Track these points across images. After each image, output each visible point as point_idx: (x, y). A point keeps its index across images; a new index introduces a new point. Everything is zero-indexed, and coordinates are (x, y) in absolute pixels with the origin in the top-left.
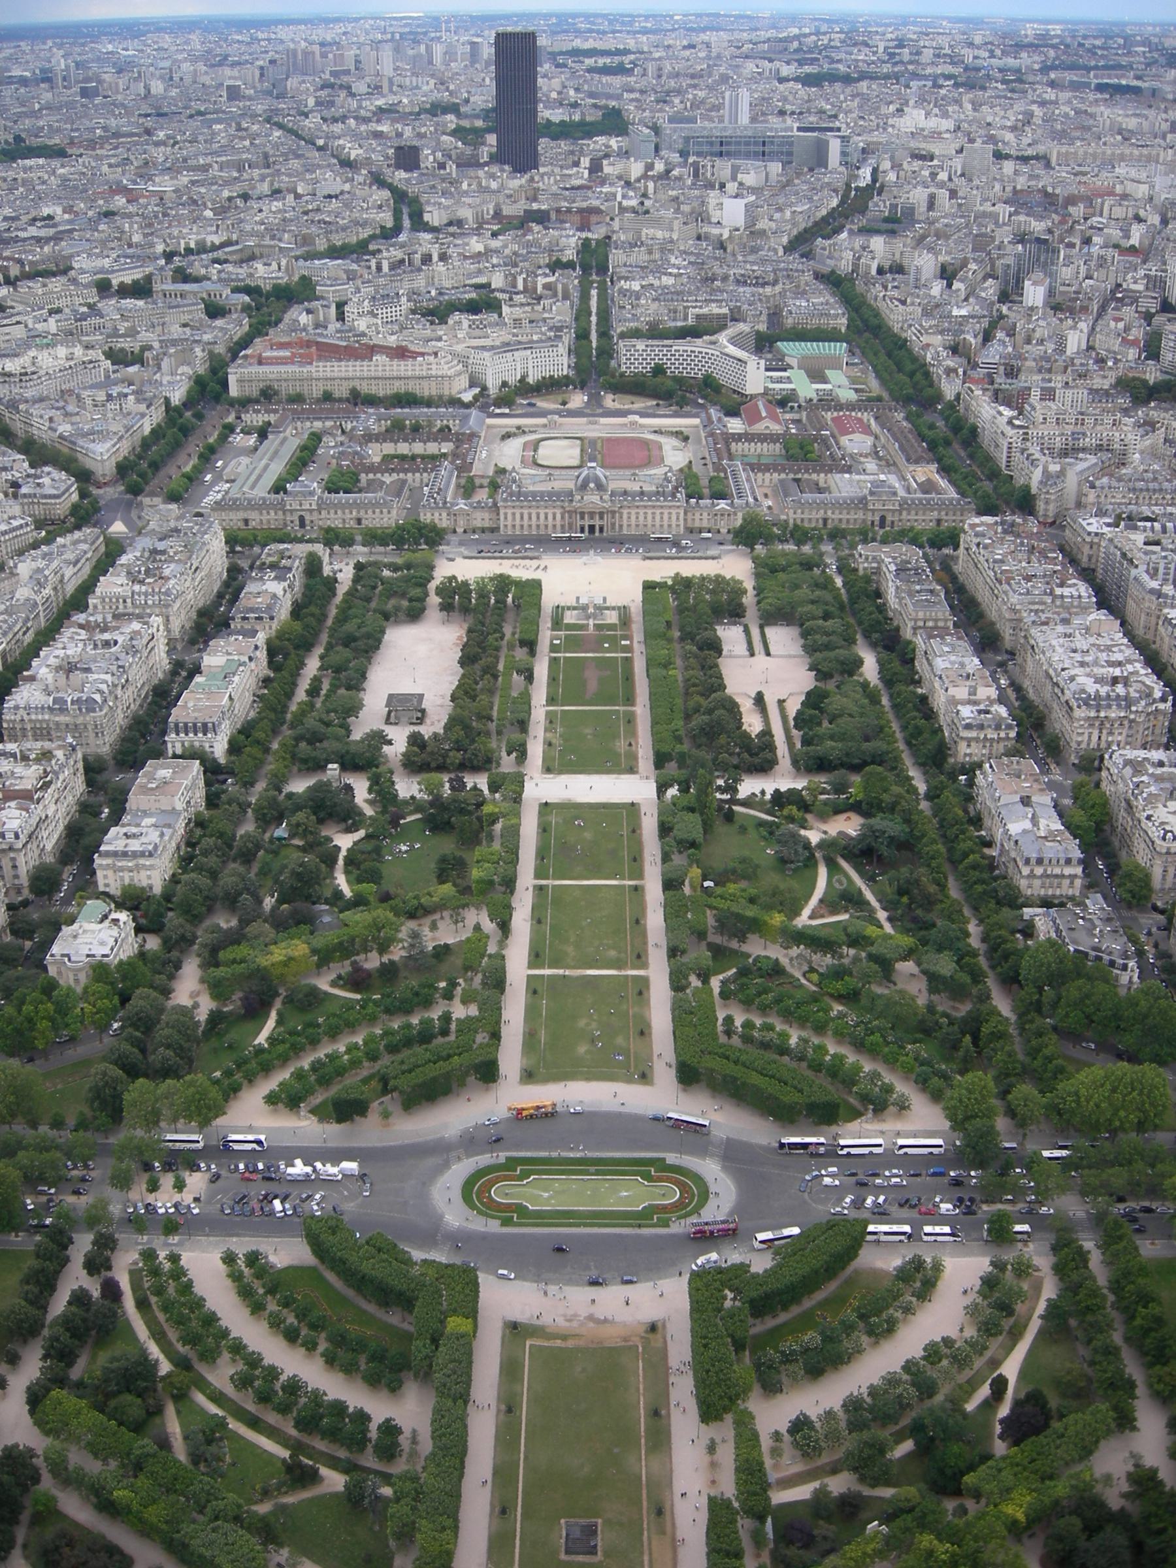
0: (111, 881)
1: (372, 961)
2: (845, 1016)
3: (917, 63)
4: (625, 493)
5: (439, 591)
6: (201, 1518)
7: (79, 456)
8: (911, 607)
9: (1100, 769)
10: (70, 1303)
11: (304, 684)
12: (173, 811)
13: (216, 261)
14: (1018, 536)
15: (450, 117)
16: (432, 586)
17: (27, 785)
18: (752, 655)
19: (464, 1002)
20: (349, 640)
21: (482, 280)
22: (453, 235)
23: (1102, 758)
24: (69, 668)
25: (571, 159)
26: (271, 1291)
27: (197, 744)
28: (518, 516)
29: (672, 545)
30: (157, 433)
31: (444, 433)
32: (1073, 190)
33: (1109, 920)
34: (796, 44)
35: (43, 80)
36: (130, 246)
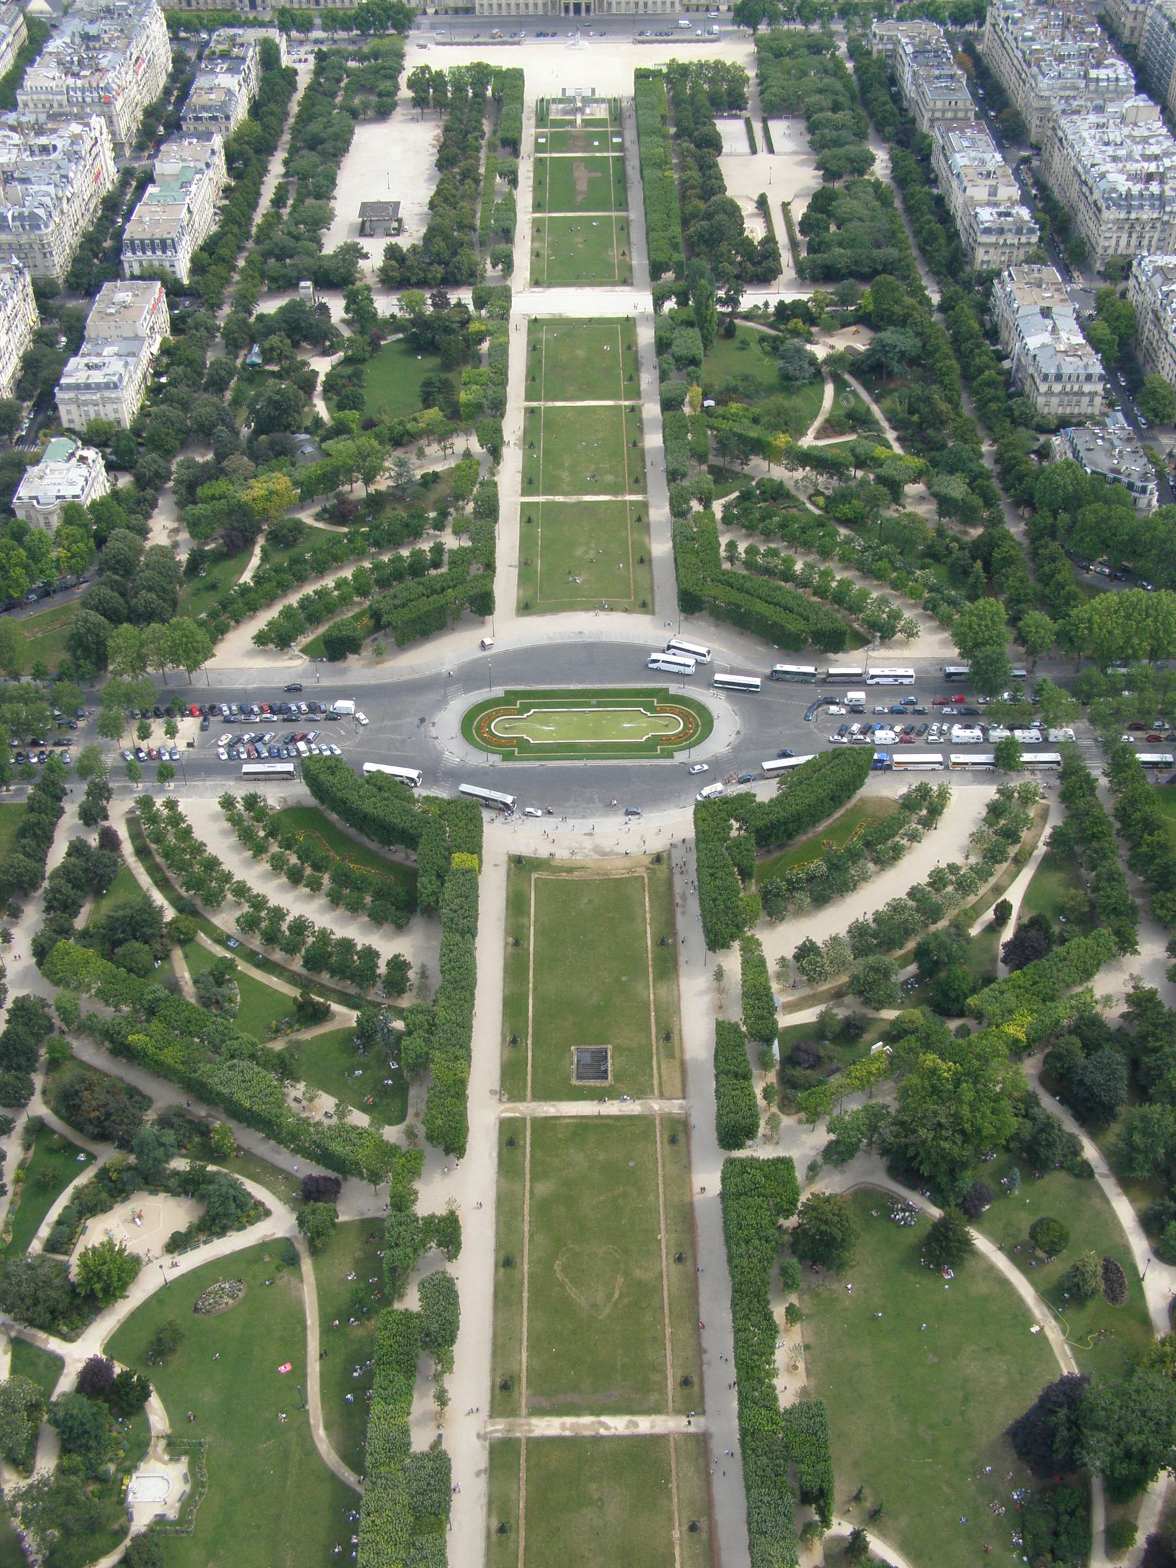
0: (75, 415)
1: (358, 490)
2: (852, 540)
5: (411, 84)
6: (218, 1058)
10: (69, 854)
11: (268, 192)
16: (403, 79)
18: (754, 151)
19: (457, 533)
23: (1130, 265)
26: (272, 834)
27: (156, 263)
29: (665, 31)
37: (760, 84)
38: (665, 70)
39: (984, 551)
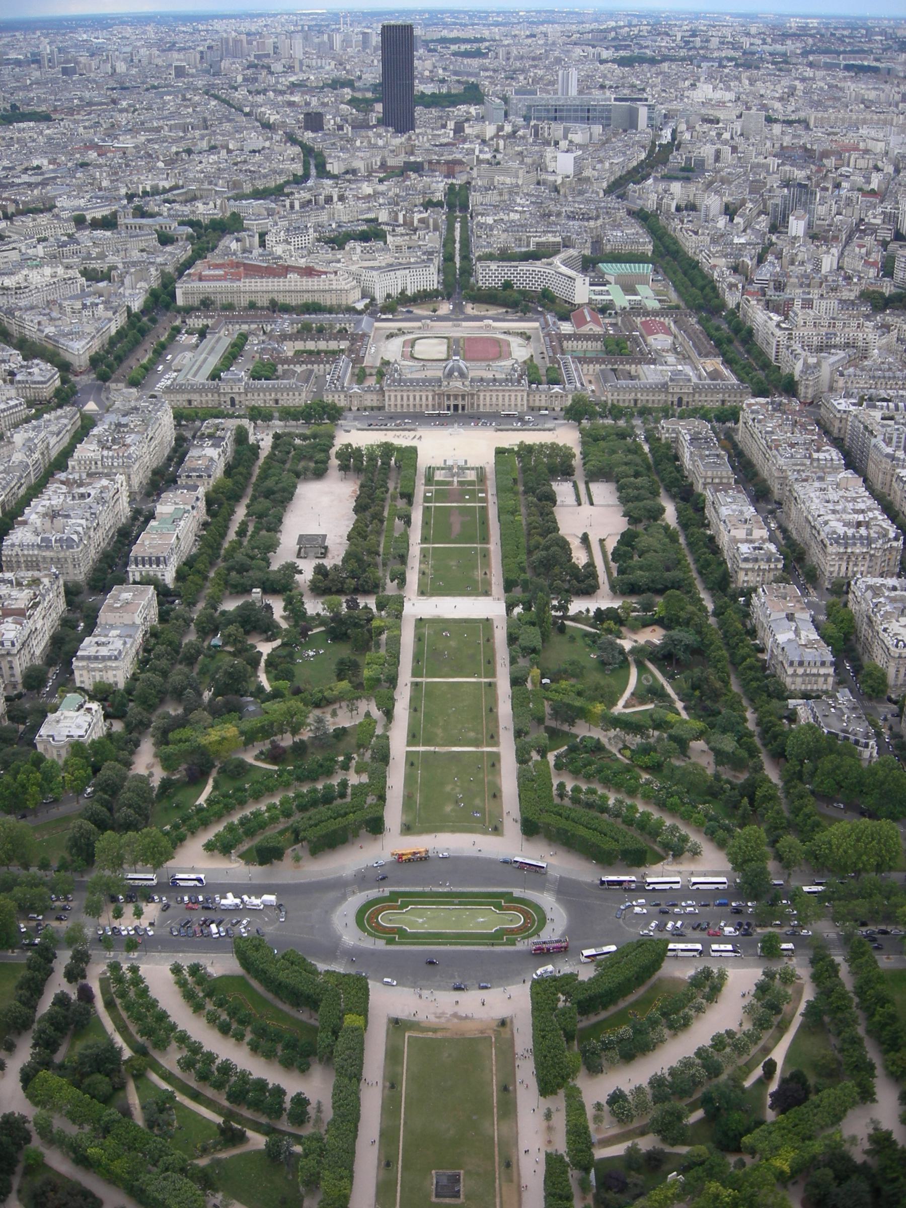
0: (85, 679)
1: (287, 741)
2: (651, 782)
3: (707, 48)
4: (482, 380)
5: (338, 456)
6: (155, 1170)
7: (61, 351)
8: (702, 468)
9: (847, 593)
10: (54, 1004)
11: (234, 527)
12: (134, 625)
13: (166, 201)
14: (784, 413)
15: (347, 90)
16: (333, 451)
17: (21, 605)
18: (580, 504)
19: (358, 772)
20: (269, 493)
21: (371, 216)
22: (349, 181)
23: (849, 584)
24: (53, 514)
25: (440, 122)
26: (209, 995)
27: (152, 573)
28: (399, 398)
29: (518, 420)
30: (121, 334)
31: (342, 334)
32: (827, 146)
33: (854, 709)
34: (613, 34)
35: (33, 62)
36: (100, 189)
37: (583, 458)
38: (516, 449)
39: (749, 790)
